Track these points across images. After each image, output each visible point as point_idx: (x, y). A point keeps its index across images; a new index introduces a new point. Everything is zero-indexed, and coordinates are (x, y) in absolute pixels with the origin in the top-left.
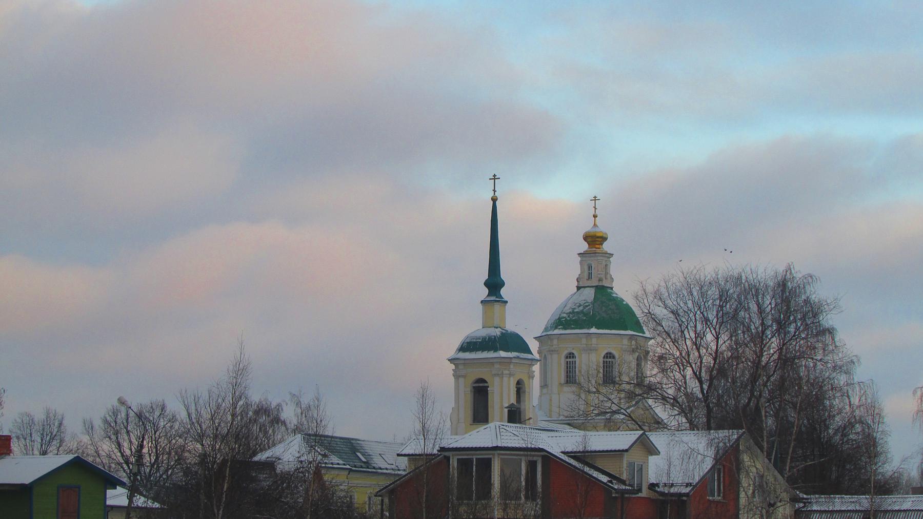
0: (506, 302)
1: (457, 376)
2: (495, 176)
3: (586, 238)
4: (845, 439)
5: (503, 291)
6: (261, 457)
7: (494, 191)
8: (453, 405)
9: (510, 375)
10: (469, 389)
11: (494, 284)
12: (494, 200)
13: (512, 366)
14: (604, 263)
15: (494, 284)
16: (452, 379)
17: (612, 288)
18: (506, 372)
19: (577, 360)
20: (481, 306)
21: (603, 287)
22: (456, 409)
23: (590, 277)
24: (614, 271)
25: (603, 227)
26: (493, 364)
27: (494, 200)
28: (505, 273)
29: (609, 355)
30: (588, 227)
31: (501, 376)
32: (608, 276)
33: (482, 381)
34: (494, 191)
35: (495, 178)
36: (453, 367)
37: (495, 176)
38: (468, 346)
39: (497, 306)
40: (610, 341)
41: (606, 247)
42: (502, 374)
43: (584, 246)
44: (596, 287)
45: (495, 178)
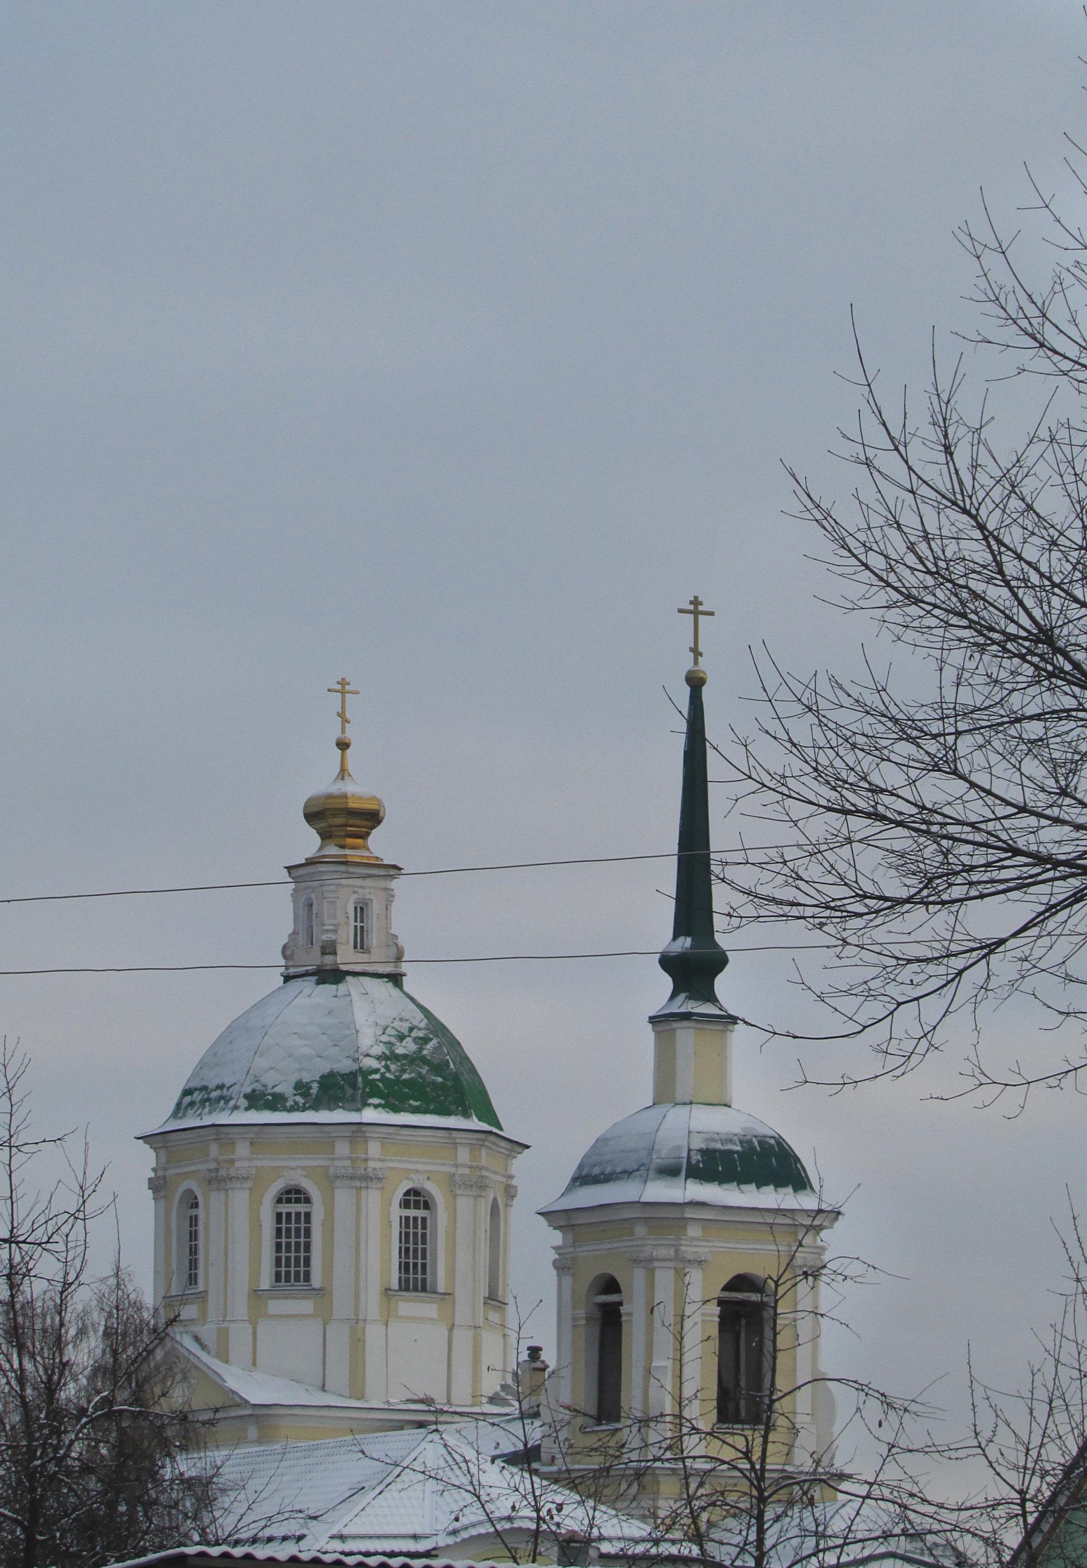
1: (562, 1267)
7: (696, 652)
10: (582, 1312)
12: (696, 683)
20: (648, 1030)
27: (696, 683)
29: (415, 1198)
31: (648, 1264)
34: (696, 652)
35: (696, 609)
41: (380, 844)
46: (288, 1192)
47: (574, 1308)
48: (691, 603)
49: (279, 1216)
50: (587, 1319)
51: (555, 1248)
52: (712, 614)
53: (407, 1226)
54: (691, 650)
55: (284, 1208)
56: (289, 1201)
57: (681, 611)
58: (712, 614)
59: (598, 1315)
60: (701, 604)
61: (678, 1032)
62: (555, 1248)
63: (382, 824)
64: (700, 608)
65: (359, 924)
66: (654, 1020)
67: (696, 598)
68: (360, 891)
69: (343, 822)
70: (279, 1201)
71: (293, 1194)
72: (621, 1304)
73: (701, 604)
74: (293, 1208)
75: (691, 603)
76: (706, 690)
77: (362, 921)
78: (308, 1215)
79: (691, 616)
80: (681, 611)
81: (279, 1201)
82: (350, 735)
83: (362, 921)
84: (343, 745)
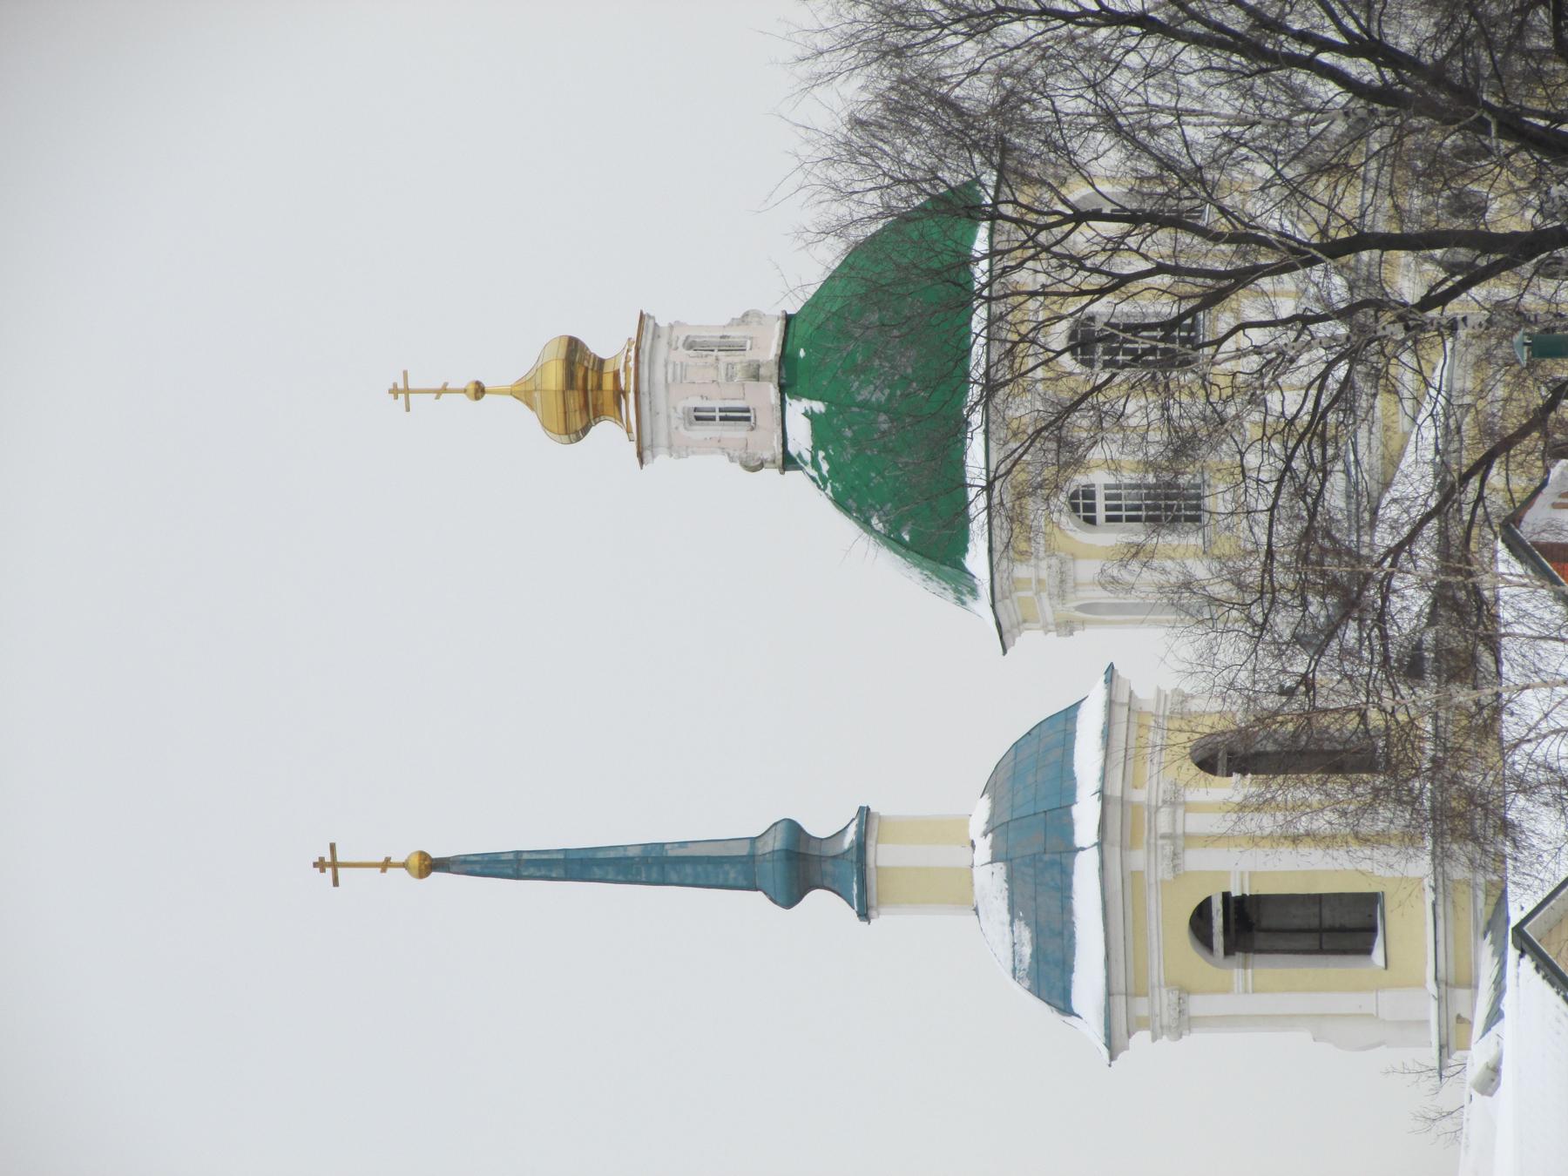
0: (865, 814)
1: (1183, 1023)
2: (320, 865)
3: (575, 431)
4: (1393, 795)
5: (818, 826)
6: (1489, 936)
7: (386, 865)
8: (1300, 1038)
9: (1175, 802)
10: (1237, 973)
11: (796, 866)
12: (430, 865)
13: (1139, 796)
14: (682, 354)
15: (796, 866)
16: (1195, 1040)
17: (789, 319)
18: (1163, 823)
21: (785, 359)
22: (1317, 1022)
23: (738, 416)
24: (709, 313)
25: (527, 351)
26: (1132, 880)
27: (430, 865)
28: (739, 817)
30: (523, 427)
32: (736, 334)
33: (1200, 919)
34: (386, 865)
35: (330, 865)
36: (1141, 1038)
37: (320, 865)
38: (1050, 977)
39: (882, 855)
40: (1025, 304)
41: (608, 342)
42: (1171, 837)
43: (608, 435)
44: (783, 388)
45: (330, 865)
46: (1075, 508)
47: (1227, 990)
48: (323, 871)
49: (1109, 519)
50: (1245, 967)
51: (1154, 1039)
52: (333, 847)
53: (1117, 519)
54: (384, 871)
55: (1101, 514)
56: (1091, 508)
57: (336, 883)
58: (333, 847)
59: (1239, 956)
60: (322, 859)
61: (879, 863)
62: (1154, 1039)
63: (581, 338)
64: (328, 859)
65: (718, 414)
66: (864, 914)
67: (315, 865)
68: (674, 422)
69: (584, 390)
70: (1091, 521)
72: (1226, 896)
73: (322, 859)
74: (1100, 503)
75: (323, 871)
76: (434, 855)
77: (722, 419)
78: (1107, 487)
79: (339, 859)
80: (336, 883)
81: (1091, 521)
82: (464, 380)
83: (722, 419)
84: (479, 391)
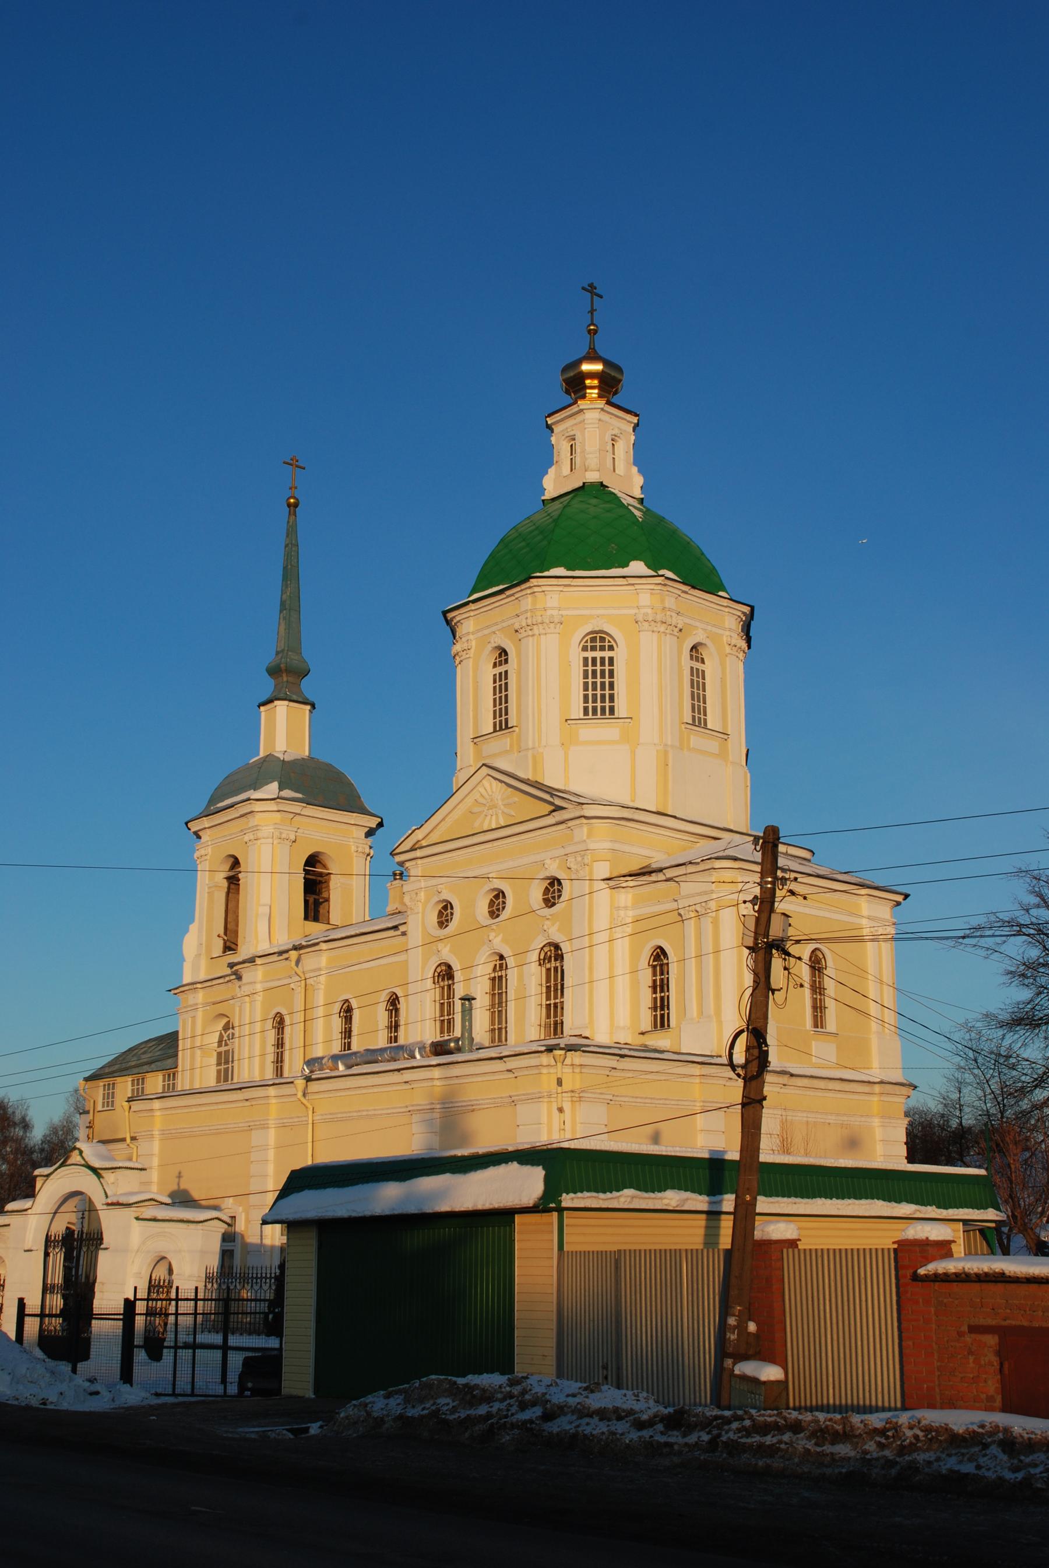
19: (620, 655)
49: (586, 659)
56: (593, 648)
70: (585, 649)
71: (598, 640)
81: (585, 649)
